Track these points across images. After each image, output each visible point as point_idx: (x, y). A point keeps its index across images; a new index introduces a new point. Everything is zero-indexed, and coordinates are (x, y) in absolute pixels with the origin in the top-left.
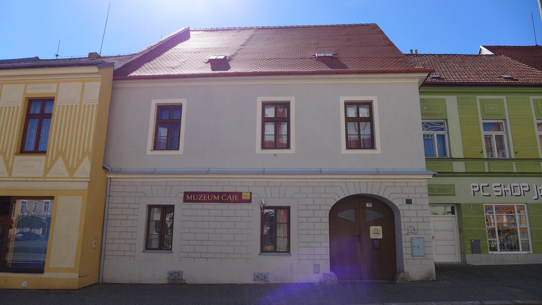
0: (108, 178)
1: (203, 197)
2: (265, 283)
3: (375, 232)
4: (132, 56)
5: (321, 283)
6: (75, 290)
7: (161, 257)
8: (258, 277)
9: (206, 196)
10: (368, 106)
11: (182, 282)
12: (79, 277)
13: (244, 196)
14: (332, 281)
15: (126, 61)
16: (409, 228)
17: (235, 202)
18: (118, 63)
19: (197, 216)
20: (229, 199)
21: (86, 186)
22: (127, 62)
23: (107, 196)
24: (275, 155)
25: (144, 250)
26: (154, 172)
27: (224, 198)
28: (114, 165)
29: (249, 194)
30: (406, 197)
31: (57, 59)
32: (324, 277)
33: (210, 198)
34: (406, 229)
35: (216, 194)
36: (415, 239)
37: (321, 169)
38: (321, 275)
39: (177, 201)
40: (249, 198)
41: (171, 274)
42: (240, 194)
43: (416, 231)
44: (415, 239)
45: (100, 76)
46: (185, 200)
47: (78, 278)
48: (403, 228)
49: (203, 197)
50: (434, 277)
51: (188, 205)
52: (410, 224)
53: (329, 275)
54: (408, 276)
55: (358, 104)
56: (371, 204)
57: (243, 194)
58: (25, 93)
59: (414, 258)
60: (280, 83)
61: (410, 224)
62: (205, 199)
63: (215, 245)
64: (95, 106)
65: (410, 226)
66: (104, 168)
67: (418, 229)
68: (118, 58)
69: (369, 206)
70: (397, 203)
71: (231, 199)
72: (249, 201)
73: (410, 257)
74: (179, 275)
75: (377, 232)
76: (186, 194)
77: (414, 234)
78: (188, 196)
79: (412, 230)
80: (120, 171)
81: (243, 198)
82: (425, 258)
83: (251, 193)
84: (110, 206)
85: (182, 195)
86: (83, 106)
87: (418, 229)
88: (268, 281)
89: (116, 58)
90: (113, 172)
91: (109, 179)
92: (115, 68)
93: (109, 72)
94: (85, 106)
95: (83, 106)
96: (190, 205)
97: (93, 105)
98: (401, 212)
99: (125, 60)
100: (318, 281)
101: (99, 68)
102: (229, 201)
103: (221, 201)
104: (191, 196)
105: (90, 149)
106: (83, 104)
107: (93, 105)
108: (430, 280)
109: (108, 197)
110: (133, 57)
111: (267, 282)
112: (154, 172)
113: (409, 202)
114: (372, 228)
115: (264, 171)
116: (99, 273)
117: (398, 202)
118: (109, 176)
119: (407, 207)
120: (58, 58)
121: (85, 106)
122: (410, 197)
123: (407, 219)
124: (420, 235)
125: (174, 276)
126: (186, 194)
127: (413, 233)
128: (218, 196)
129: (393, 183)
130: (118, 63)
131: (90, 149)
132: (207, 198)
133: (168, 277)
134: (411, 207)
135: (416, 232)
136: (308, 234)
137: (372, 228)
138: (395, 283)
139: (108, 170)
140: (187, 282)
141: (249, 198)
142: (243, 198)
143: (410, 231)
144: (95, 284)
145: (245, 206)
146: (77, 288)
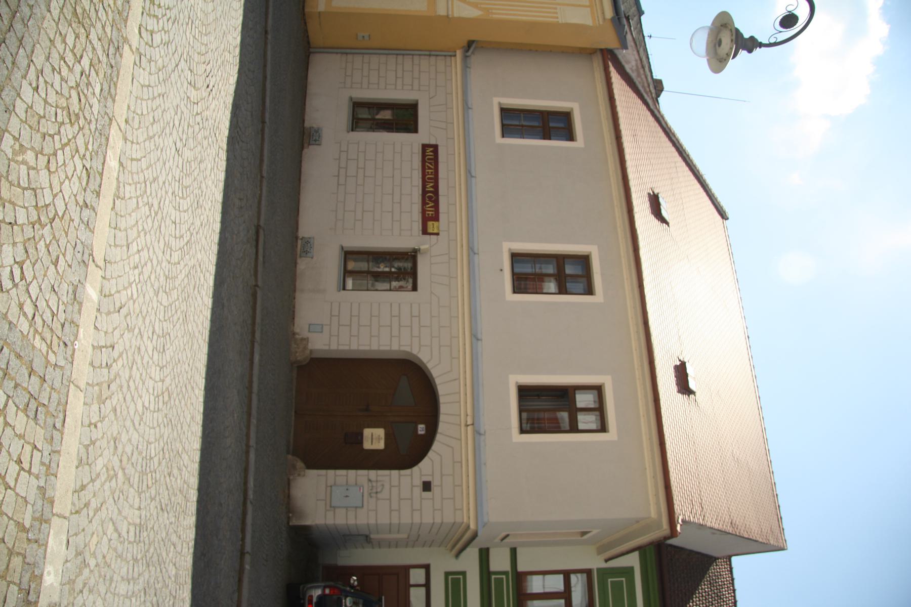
0: (455, 52)
1: (431, 169)
2: (298, 253)
3: (374, 437)
4: (649, 94)
5: (294, 334)
6: (304, 7)
7: (344, 116)
8: (308, 242)
9: (432, 172)
10: (599, 428)
11: (306, 145)
12: (319, 13)
13: (433, 224)
14: (296, 352)
15: (640, 83)
16: (379, 484)
17: (424, 212)
18: (633, 66)
19: (401, 163)
20: (428, 204)
21: (442, 12)
22: (637, 83)
23: (430, 53)
24: (501, 270)
25: (345, 249)
26: (466, 107)
27: (430, 198)
28: (476, 59)
29: (435, 231)
30: (435, 483)
31: (644, 37)
32: (302, 339)
33: (429, 178)
34: (379, 478)
35: (436, 187)
36: (362, 491)
37: (481, 340)
38: (305, 334)
39: (425, 134)
40: (430, 231)
41: (318, 131)
42: (436, 218)
43: (374, 495)
44: (362, 491)
45: (601, 23)
46: (425, 147)
47: (319, 11)
48: (380, 472)
49: (430, 168)
50: (294, 522)
51: (418, 150)
52: (387, 486)
53: (305, 348)
54: (299, 475)
55: (600, 409)
56: (423, 433)
57: (436, 224)
58: (615, 49)
59: (329, 489)
60: (625, 281)
61: (387, 486)
62: (428, 172)
63: (351, 336)
64: (557, 20)
65: (383, 485)
66: (470, 44)
67: (377, 499)
68: (640, 66)
69: (419, 429)
70: (425, 464)
71: (428, 206)
72: (425, 232)
73: (331, 482)
74: (315, 140)
75: (374, 441)
76: (435, 148)
77: (370, 491)
78: (431, 149)
79: (377, 489)
80: (467, 67)
81: (430, 223)
82: (328, 508)
83: (437, 234)
84: (416, 58)
85: (433, 142)
86: (555, 6)
87: (377, 499)
88: (301, 257)
89: (639, 62)
90: (465, 57)
91: (453, 54)
92: (616, 52)
93: (609, 41)
94: (556, 9)
95: (555, 6)
96: (417, 152)
97: (557, 18)
98: (408, 472)
99: (639, 79)
100: (297, 330)
101: (612, 19)
102: (424, 203)
103: (424, 192)
104: (431, 154)
105: (494, 16)
106: (558, 7)
107: (557, 18)
108: (291, 515)
109: (427, 53)
110: (648, 96)
111: (298, 256)
112: (466, 107)
113: (427, 486)
114: (380, 432)
115: (467, 67)
116: (324, 48)
117: (425, 468)
118: (459, 53)
119: (418, 482)
120: (647, 39)
121: (556, 9)
122: (435, 489)
123: (395, 482)
124: (368, 502)
125: (315, 134)
126: (435, 148)
127: (371, 490)
128: (431, 189)
129: (460, 460)
130: (633, 66)
131: (494, 16)
132: (428, 175)
133: (313, 128)
134: (418, 490)
135: (372, 495)
136: (371, 316)
137: (380, 432)
138: (288, 453)
139: (467, 51)
140: (305, 151)
141: (430, 231)
142: (430, 223)
143: (374, 484)
144: (309, 43)
145: (417, 226)
146: (307, 10)
